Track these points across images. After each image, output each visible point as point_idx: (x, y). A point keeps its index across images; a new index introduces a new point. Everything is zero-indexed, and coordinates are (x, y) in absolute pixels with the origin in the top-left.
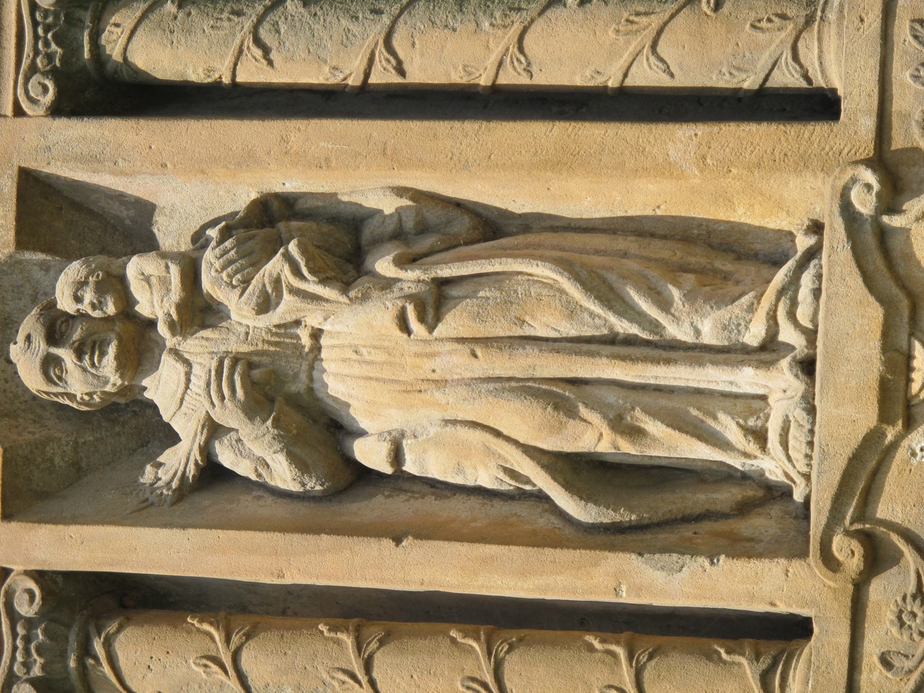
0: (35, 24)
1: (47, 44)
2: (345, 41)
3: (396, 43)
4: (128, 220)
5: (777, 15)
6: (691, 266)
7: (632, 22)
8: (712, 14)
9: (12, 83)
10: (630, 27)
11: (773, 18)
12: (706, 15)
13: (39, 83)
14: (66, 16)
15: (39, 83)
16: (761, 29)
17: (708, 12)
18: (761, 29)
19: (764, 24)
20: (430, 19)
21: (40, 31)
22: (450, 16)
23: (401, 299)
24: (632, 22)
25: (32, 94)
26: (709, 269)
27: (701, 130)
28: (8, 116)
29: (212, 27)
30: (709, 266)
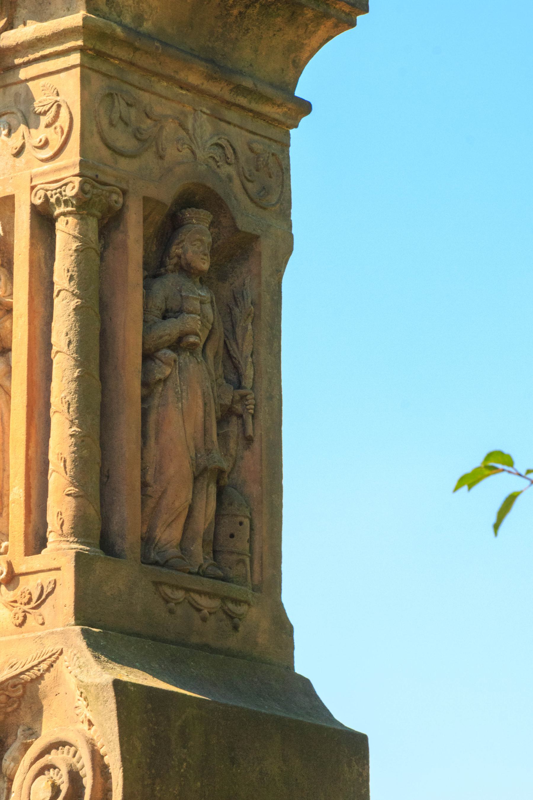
0: (61, 187)
1: (56, 194)
2: (60, 332)
3: (59, 354)
4: (288, 120)
5: (63, 521)
6: (3, 499)
7: (61, 459)
8: (64, 493)
9: (41, 182)
10: (60, 459)
11: (62, 520)
12: (64, 491)
13: (41, 195)
14: (66, 200)
15: (41, 195)
16: (58, 516)
17: (65, 492)
18: (58, 516)
19: (60, 517)
20: (66, 369)
21: (59, 190)
22: (67, 377)
23: (191, 309)
24: (61, 459)
25: (38, 192)
26: (3, 506)
27: (23, 499)
28: (31, 183)
29: (64, 269)
30: (4, 506)
